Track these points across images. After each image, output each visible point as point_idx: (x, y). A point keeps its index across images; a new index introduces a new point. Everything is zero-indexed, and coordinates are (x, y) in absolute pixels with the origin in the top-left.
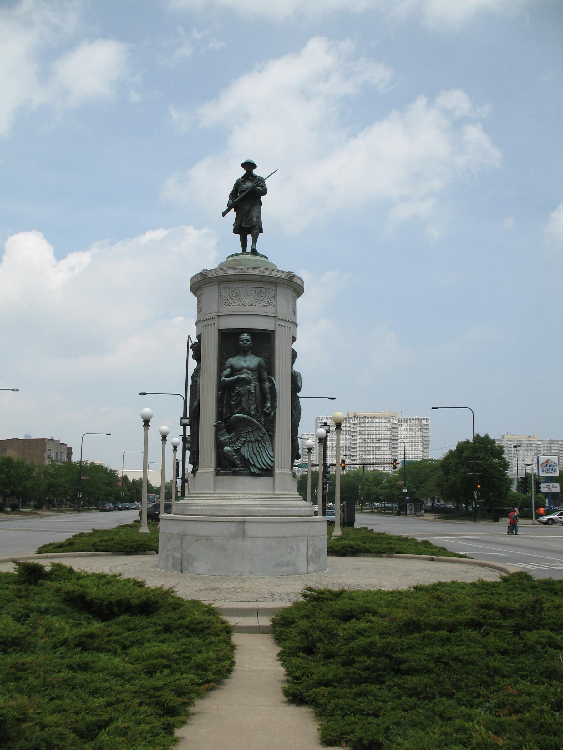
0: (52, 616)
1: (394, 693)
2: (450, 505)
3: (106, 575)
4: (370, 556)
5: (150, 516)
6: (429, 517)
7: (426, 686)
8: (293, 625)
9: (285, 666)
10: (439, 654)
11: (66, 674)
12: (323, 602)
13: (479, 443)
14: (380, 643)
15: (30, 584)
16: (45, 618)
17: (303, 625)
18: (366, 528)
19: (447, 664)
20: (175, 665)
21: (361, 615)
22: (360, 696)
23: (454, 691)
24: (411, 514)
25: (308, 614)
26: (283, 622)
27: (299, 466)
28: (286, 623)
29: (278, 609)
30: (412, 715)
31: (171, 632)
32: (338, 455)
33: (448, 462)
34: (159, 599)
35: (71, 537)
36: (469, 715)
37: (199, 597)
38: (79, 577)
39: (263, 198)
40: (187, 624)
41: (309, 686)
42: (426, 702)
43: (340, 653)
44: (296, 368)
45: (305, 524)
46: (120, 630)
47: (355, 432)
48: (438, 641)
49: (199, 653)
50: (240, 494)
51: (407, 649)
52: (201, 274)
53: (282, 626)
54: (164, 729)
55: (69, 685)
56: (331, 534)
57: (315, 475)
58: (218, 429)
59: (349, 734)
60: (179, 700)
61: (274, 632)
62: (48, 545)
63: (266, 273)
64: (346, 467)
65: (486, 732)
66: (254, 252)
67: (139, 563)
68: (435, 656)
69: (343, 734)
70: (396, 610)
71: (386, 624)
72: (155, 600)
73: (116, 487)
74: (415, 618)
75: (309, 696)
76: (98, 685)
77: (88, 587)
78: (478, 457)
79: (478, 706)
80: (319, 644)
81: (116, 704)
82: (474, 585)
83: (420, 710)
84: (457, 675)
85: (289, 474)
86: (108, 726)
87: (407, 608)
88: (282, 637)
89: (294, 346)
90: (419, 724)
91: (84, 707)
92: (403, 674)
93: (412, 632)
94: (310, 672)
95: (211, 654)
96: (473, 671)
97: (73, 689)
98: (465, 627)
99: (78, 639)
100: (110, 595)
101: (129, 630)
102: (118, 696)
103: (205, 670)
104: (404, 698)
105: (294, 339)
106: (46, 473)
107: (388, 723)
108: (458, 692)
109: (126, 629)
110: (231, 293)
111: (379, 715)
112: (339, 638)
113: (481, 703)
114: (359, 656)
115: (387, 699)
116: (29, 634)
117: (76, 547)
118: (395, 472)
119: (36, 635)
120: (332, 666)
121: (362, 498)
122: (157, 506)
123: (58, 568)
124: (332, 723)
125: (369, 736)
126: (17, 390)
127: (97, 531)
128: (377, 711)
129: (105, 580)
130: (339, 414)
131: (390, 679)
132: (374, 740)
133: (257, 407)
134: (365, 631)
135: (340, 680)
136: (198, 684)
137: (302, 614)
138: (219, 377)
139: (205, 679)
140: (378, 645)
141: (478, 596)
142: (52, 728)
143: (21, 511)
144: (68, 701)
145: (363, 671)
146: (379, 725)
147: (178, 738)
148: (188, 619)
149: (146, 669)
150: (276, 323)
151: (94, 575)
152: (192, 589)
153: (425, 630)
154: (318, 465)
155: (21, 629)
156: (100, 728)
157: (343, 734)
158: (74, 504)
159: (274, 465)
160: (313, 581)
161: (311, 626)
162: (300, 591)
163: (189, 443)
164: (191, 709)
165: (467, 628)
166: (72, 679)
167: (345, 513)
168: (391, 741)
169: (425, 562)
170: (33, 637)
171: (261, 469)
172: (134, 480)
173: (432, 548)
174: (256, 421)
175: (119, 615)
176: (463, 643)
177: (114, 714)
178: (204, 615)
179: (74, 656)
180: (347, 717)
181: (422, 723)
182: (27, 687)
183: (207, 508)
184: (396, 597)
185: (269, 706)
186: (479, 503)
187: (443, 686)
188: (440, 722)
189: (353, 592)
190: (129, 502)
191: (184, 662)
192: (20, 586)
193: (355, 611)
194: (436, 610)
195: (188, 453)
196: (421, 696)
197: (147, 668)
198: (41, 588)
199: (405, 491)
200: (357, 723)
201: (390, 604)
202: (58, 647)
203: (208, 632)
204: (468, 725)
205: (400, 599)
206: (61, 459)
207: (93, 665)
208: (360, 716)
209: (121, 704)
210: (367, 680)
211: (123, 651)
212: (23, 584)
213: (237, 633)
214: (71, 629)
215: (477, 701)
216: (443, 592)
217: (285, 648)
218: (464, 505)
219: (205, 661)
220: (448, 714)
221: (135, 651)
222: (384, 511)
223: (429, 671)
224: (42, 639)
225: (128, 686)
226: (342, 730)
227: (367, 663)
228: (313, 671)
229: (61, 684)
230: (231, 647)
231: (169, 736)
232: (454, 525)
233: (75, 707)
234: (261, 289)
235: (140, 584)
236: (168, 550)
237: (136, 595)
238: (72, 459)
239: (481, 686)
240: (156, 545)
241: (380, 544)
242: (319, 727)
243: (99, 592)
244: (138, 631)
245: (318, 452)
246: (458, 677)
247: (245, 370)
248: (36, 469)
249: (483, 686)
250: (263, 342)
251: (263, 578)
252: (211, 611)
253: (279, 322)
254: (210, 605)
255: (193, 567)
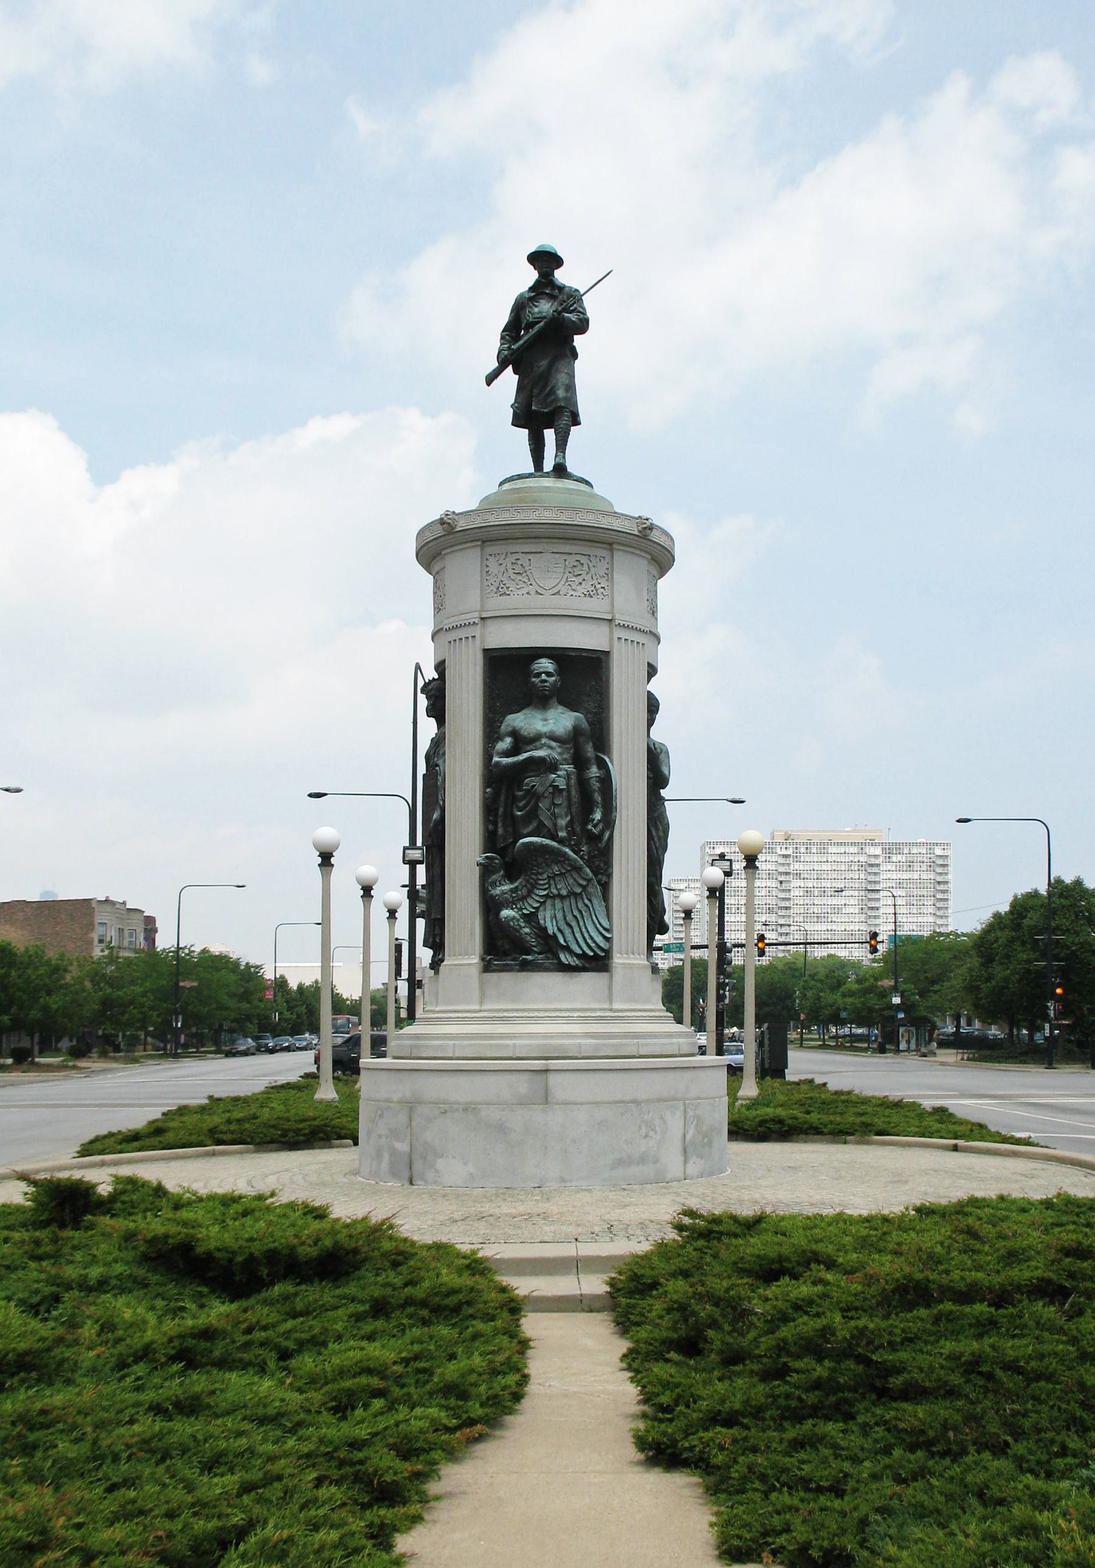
0: (115, 1295)
1: (876, 1441)
2: (994, 1032)
3: (240, 1197)
4: (821, 1141)
5: (338, 1064)
6: (949, 1056)
7: (945, 1426)
8: (654, 1292)
9: (638, 1382)
10: (973, 1354)
11: (146, 1426)
12: (719, 1240)
13: (1061, 896)
14: (842, 1327)
15: (63, 1226)
16: (99, 1301)
17: (676, 1292)
18: (811, 1081)
19: (990, 1377)
20: (397, 1389)
21: (801, 1269)
22: (802, 1446)
23: (1009, 1438)
24: (908, 1050)
25: (686, 1266)
26: (632, 1285)
27: (666, 948)
28: (640, 1287)
29: (621, 1257)
30: (914, 1492)
31: (388, 1316)
32: (750, 923)
33: (991, 937)
34: (360, 1243)
35: (159, 1116)
36: (1043, 1495)
37: (450, 1236)
38: (178, 1205)
39: (578, 341)
40: (423, 1296)
41: (692, 1426)
42: (947, 1461)
43: (757, 1352)
44: (658, 734)
45: (678, 1075)
46: (274, 1317)
47: (787, 874)
48: (970, 1325)
49: (450, 1360)
50: (538, 1010)
51: (902, 1343)
52: (441, 521)
53: (631, 1293)
54: (372, 1537)
55: (153, 1452)
56: (735, 1095)
57: (699, 967)
58: (486, 870)
59: (779, 1533)
60: (407, 1467)
61: (614, 1308)
62: (105, 1137)
63: (589, 520)
64: (767, 949)
65: (1084, 1538)
66: (560, 471)
67: (314, 1167)
68: (963, 1359)
69: (765, 1534)
70: (877, 1256)
71: (856, 1287)
72: (353, 1245)
73: (261, 1001)
74: (919, 1276)
75: (692, 1448)
76: (223, 1444)
77: (200, 1226)
78: (1058, 928)
79: (1063, 1476)
80: (710, 1333)
81: (264, 1486)
82: (1047, 1204)
83: (934, 1481)
84: (1013, 1402)
85: (644, 965)
86: (243, 1539)
87: (901, 1254)
88: (632, 1317)
89: (655, 686)
90: (931, 1512)
91: (190, 1499)
92: (894, 1399)
93: (911, 1306)
94: (692, 1395)
95: (477, 1360)
96: (1048, 1395)
97: (163, 1460)
98: (1028, 1296)
99: (176, 1343)
100: (251, 1240)
101: (295, 1315)
102: (269, 1467)
103: (464, 1396)
104: (897, 1453)
105: (652, 671)
106: (97, 976)
107: (864, 1509)
108: (1016, 1441)
109: (287, 1314)
110: (509, 566)
111: (844, 1492)
112: (754, 1319)
113: (1070, 1468)
114: (798, 1357)
115: (861, 1455)
116: (60, 1340)
117: (170, 1137)
118: (874, 961)
119: (76, 1342)
120: (740, 1382)
121: (802, 1016)
122: (354, 1042)
123: (129, 1187)
124: (742, 1508)
125: (823, 1539)
126: (19, 791)
127: (219, 1099)
128: (838, 1481)
129: (239, 1208)
130: (753, 836)
131: (867, 1410)
132: (834, 1547)
133: (571, 822)
134: (811, 1302)
135: (758, 1412)
136: (449, 1430)
137: (674, 1267)
138: (488, 756)
139: (464, 1416)
140: (840, 1334)
141: (1057, 1230)
142: (111, 1559)
143: (38, 1065)
144: (150, 1488)
145: (807, 1391)
146: (843, 1514)
147: (403, 1555)
148: (426, 1284)
149: (331, 1401)
150: (611, 633)
151: (212, 1197)
152: (433, 1220)
153: (942, 1302)
154: (706, 947)
155: (43, 1329)
156: (224, 1545)
157: (765, 1534)
158: (165, 1042)
159: (611, 947)
160: (697, 1197)
161: (694, 1293)
162: (668, 1218)
163: (422, 902)
164: (433, 1488)
165: (1033, 1297)
166: (160, 1436)
167: (766, 1048)
168: (873, 1552)
169: (940, 1153)
170: (68, 1346)
171: (583, 956)
172: (301, 987)
173: (955, 1123)
174: (571, 853)
175: (272, 1283)
176: (1026, 1331)
177: (257, 1510)
178: (460, 1276)
179: (167, 1384)
180: (773, 1496)
181: (938, 1511)
182: (53, 1465)
183: (465, 1042)
184: (876, 1229)
185: (605, 1472)
186: (1058, 1027)
187: (984, 1427)
188: (980, 1510)
189: (783, 1218)
190: (292, 1035)
191: (417, 1382)
192: (37, 1234)
193: (788, 1259)
194: (965, 1257)
195: (421, 923)
196: (934, 1449)
197: (334, 1399)
198: (90, 1233)
199: (896, 1000)
200: (797, 1510)
201: (864, 1244)
202: (129, 1366)
203: (471, 1311)
204: (1043, 1518)
205: (885, 1234)
206: (130, 942)
207: (211, 1401)
208: (802, 1494)
209: (275, 1484)
210: (815, 1411)
211: (281, 1364)
212: (44, 1228)
213: (534, 1311)
214: (160, 1322)
215: (1060, 1463)
216: (980, 1219)
217: (637, 1341)
218: (1025, 1032)
219: (463, 1376)
220: (995, 1492)
221: (307, 1362)
222: (850, 1045)
223: (952, 1393)
224: (90, 1348)
225: (291, 1442)
226: (763, 1525)
227: (816, 1374)
228: (698, 1392)
229: (134, 1450)
230: (520, 1342)
231: (384, 1553)
232: (996, 1073)
233: (167, 1502)
234: (578, 557)
235: (319, 1214)
236: (380, 1136)
237: (309, 1237)
238: (157, 944)
239: (1069, 1429)
240: (352, 1126)
241: (841, 1114)
242: (714, 1519)
243: (226, 1235)
244: (315, 1317)
245: (707, 918)
246: (1016, 1407)
247: (544, 741)
248: (70, 968)
249: (1073, 1430)
250: (582, 676)
251: (590, 1191)
252: (476, 1266)
253: (619, 633)
254: (474, 1252)
255: (437, 1171)
